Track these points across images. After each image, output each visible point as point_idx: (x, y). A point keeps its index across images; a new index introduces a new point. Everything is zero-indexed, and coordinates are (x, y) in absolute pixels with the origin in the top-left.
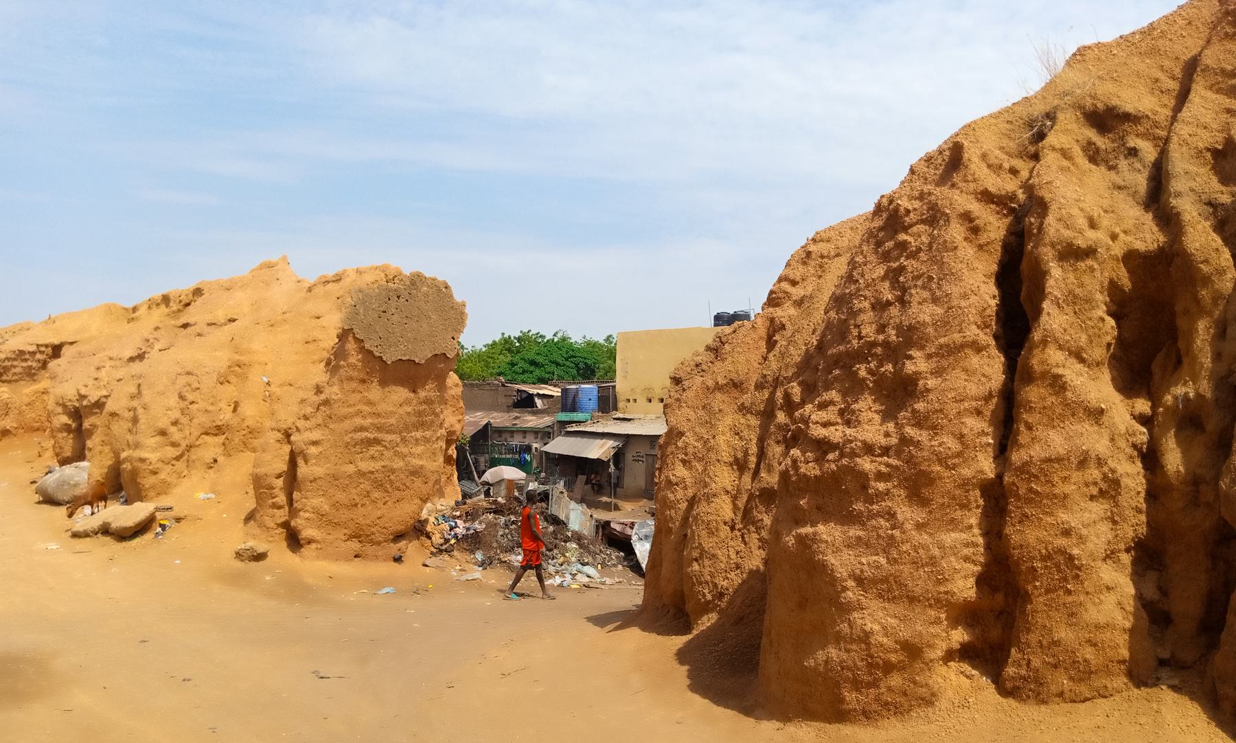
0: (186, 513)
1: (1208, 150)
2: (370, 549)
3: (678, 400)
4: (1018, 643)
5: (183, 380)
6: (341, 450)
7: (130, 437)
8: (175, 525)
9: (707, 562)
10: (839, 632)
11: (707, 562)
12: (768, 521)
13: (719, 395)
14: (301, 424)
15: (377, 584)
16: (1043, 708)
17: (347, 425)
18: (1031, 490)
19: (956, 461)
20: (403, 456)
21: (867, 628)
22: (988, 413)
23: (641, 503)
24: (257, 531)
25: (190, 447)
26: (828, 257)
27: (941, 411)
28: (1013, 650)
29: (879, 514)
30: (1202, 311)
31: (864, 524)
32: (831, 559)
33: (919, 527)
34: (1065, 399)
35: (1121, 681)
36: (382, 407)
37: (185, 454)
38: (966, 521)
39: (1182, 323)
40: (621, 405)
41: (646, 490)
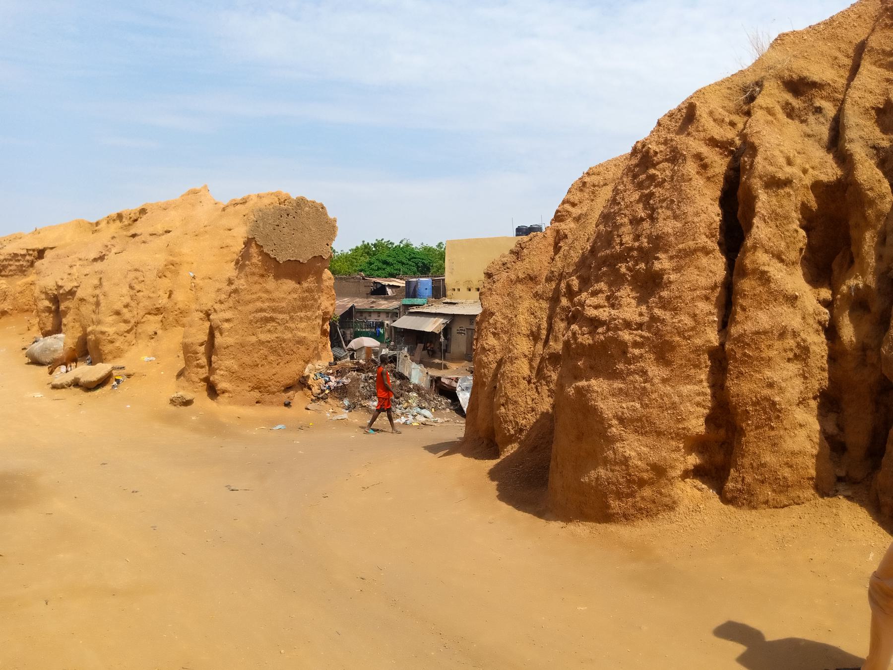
0: (134, 371)
1: (873, 108)
2: (267, 397)
3: (490, 289)
7: (94, 316)
8: (126, 379)
9: (511, 407)
10: (606, 457)
12: (555, 377)
13: (519, 286)
14: (218, 306)
15: (272, 422)
16: (754, 512)
17: (251, 307)
18: (745, 354)
19: (691, 333)
20: (291, 330)
21: (627, 454)
22: (714, 299)
23: (463, 364)
24: (186, 384)
25: (137, 323)
26: (598, 186)
27: (680, 297)
28: (732, 470)
30: (868, 225)
31: (624, 379)
32: (601, 404)
33: (664, 381)
34: (770, 289)
35: (810, 493)
39: (854, 233)
40: (449, 293)
41: (467, 355)
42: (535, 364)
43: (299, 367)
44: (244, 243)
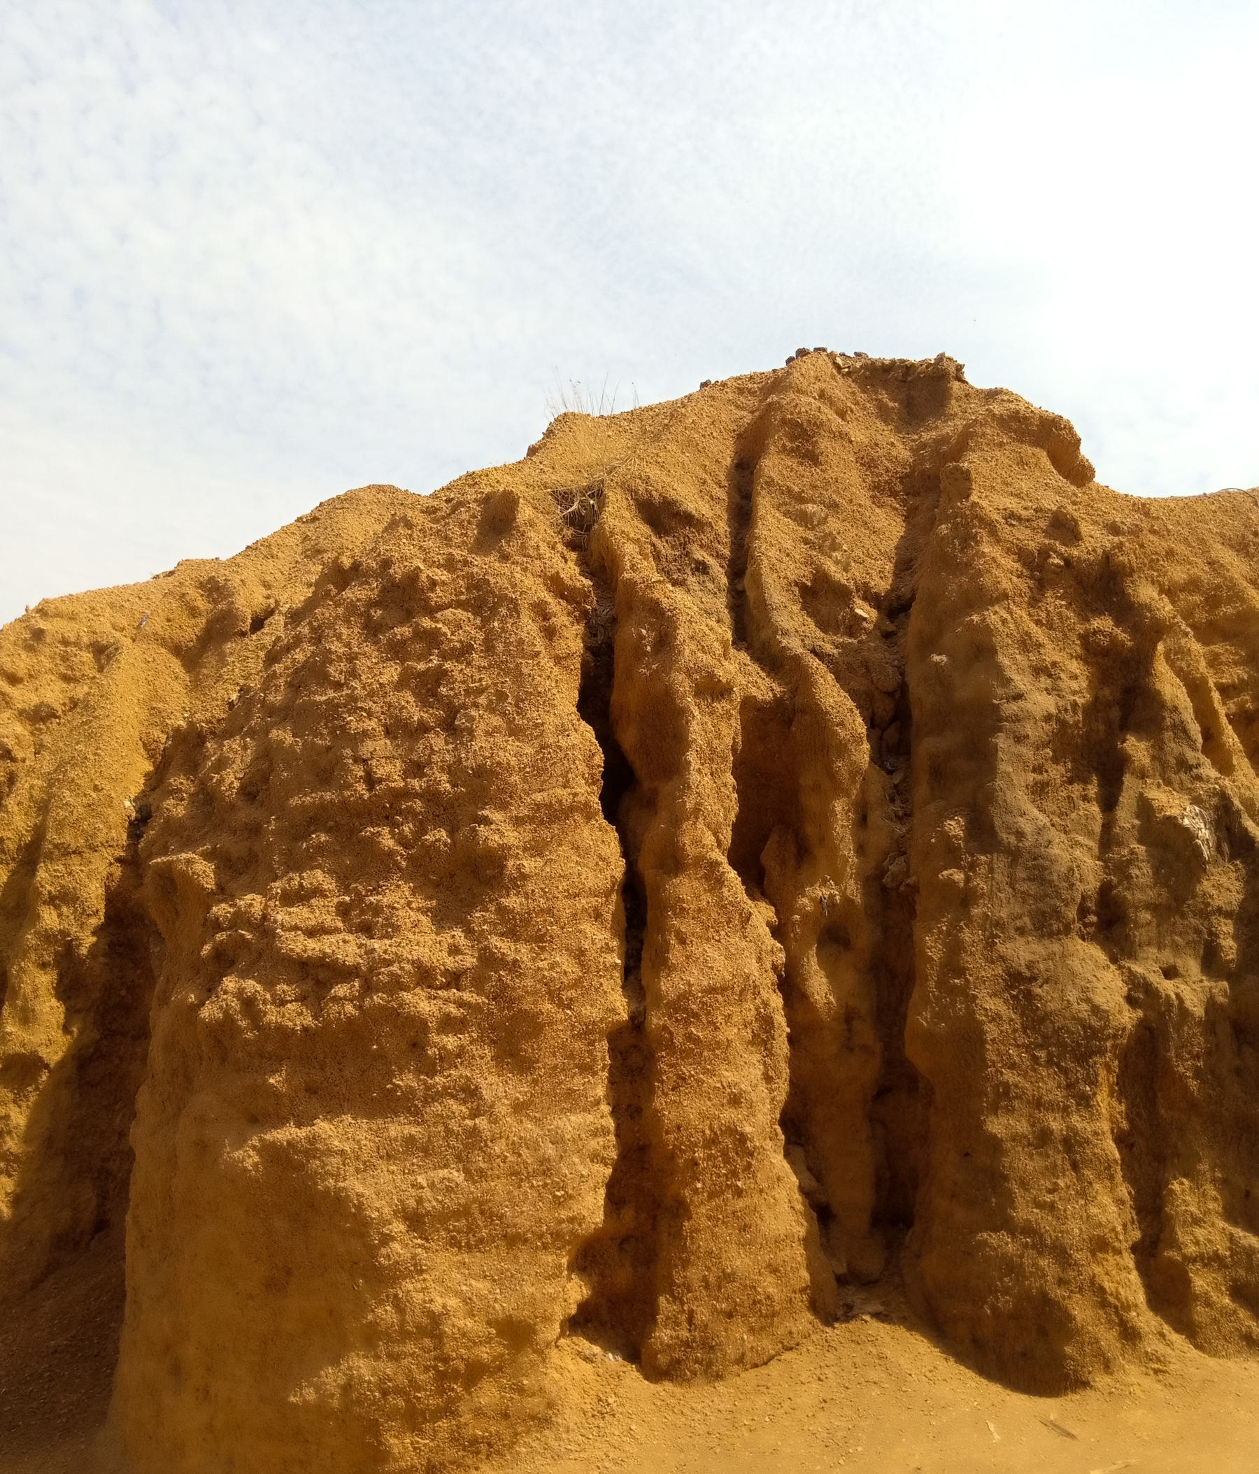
1: (796, 584)
4: (670, 1288)
10: (373, 1325)
16: (721, 1387)
18: (690, 1037)
19: (572, 993)
21: (437, 1308)
22: (609, 917)
26: (76, 644)
27: (550, 911)
28: (662, 1301)
29: (446, 1093)
30: (838, 789)
31: (417, 1113)
32: (355, 1185)
33: (519, 1108)
34: (721, 899)
35: (805, 1320)
38: (590, 1093)
39: (811, 802)
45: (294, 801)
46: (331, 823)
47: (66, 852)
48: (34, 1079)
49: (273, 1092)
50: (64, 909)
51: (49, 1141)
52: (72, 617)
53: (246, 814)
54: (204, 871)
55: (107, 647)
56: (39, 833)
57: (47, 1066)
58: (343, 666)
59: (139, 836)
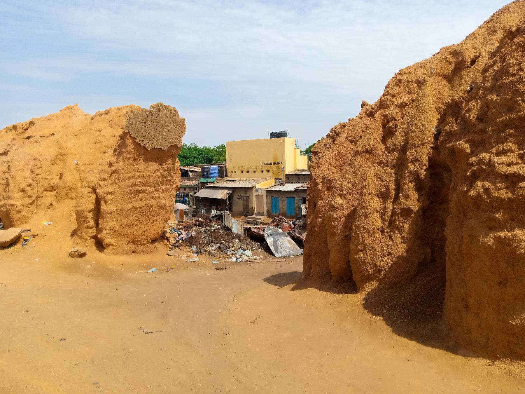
0: (38, 232)
2: (140, 248)
3: (316, 163)
5: (32, 163)
6: (125, 196)
7: (5, 194)
8: (32, 239)
9: (369, 252)
11: (369, 252)
12: (406, 227)
13: (359, 158)
14: (102, 183)
15: (147, 267)
17: (127, 183)
20: (156, 199)
23: (241, 218)
24: (79, 241)
25: (37, 198)
26: (412, 82)
36: (145, 173)
37: (35, 201)
40: (229, 174)
41: (243, 212)
42: (387, 217)
43: (162, 225)
44: (120, 136)
45: (498, 119)
46: (514, 126)
47: (415, 146)
48: (410, 216)
49: (497, 220)
50: (416, 164)
51: (416, 234)
52: (409, 73)
53: (480, 126)
54: (466, 147)
55: (421, 81)
56: (406, 141)
57: (414, 212)
58: (516, 67)
59: (438, 139)
